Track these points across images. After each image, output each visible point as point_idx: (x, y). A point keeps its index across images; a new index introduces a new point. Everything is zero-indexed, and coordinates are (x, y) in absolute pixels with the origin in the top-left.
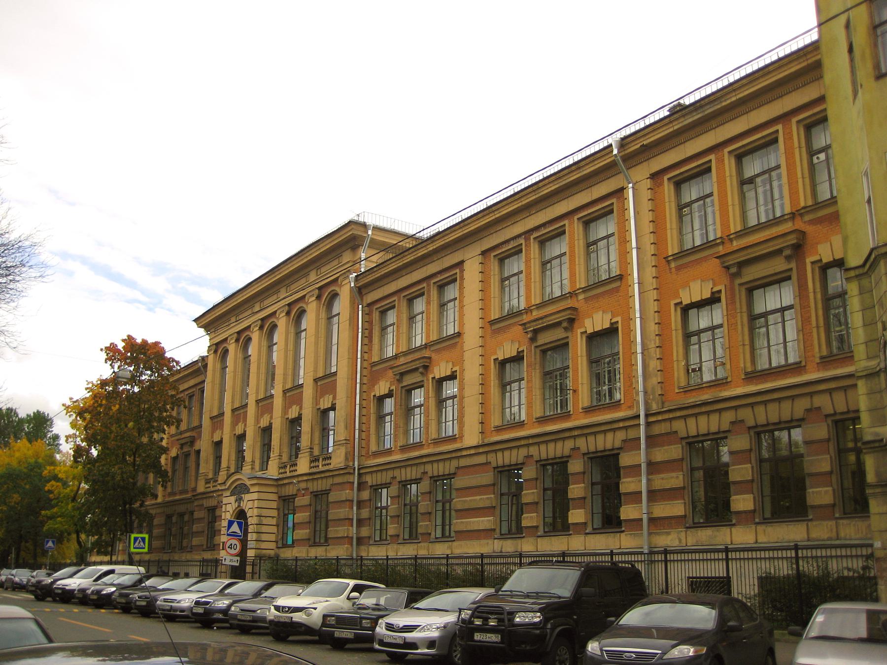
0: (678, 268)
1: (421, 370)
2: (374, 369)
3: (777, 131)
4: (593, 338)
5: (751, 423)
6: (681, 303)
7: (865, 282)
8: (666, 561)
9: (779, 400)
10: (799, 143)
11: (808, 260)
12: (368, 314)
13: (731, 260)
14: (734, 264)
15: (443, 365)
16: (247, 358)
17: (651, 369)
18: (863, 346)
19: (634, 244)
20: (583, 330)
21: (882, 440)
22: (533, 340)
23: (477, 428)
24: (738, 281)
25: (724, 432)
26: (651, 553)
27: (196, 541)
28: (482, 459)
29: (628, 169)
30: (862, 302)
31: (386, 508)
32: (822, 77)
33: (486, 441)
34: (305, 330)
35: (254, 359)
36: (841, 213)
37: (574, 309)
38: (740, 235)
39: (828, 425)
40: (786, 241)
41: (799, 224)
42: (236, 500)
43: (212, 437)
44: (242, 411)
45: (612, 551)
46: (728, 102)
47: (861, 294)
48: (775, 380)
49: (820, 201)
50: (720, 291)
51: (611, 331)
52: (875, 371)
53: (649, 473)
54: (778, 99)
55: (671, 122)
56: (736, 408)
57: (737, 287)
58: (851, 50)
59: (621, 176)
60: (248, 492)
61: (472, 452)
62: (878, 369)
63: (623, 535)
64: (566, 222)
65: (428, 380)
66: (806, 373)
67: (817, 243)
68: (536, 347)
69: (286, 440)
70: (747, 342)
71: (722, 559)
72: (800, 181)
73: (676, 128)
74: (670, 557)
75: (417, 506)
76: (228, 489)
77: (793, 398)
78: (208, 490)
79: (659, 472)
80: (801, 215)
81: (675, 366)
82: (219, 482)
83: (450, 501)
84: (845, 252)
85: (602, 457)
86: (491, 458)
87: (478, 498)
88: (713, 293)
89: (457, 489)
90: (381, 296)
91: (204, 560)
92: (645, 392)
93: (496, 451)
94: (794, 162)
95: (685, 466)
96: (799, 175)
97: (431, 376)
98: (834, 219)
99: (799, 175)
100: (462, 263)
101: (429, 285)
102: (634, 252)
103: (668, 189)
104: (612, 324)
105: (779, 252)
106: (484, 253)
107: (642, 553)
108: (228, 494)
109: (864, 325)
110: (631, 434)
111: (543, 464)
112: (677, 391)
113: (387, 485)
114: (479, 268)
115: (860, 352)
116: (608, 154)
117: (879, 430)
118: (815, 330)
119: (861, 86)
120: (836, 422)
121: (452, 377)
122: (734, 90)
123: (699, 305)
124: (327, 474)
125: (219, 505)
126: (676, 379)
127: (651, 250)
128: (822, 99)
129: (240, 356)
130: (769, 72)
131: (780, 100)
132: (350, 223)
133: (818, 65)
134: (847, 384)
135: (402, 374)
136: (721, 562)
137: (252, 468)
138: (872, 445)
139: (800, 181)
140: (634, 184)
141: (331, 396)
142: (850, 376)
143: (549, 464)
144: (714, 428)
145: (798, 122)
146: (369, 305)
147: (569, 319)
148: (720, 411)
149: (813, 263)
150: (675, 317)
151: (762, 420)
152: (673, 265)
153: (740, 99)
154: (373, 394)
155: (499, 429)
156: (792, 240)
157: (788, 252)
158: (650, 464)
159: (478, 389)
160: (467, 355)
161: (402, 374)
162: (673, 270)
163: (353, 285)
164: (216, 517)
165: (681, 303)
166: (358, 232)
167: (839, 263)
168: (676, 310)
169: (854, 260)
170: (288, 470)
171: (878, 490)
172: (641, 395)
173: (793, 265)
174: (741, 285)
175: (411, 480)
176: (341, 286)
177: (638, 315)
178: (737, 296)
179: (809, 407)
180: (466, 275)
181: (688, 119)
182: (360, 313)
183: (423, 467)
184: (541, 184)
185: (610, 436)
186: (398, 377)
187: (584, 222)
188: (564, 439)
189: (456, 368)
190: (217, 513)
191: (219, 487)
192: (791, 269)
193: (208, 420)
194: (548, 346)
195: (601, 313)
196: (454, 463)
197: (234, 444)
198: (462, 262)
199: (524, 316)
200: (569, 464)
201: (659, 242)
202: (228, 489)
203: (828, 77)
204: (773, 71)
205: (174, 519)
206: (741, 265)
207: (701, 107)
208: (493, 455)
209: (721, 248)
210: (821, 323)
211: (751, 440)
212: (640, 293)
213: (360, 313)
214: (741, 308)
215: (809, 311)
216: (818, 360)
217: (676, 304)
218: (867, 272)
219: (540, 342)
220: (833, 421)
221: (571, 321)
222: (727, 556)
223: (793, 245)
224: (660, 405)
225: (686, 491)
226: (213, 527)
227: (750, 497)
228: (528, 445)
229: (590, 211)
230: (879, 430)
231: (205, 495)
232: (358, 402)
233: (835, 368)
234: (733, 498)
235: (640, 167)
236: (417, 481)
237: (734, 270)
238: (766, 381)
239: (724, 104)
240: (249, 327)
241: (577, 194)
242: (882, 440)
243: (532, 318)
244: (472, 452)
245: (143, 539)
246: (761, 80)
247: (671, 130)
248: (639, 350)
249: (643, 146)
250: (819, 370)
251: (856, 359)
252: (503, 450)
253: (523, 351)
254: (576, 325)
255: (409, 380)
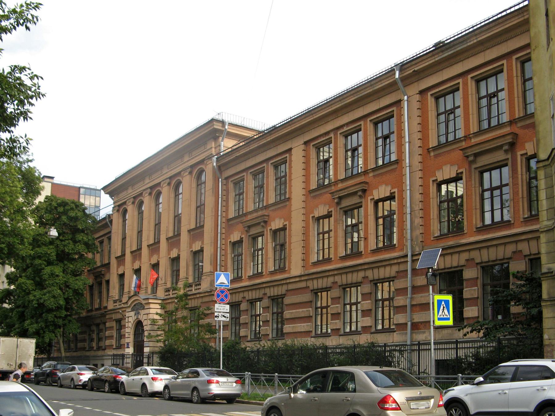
0: (436, 156)
1: (262, 224)
2: (230, 223)
3: (503, 64)
4: (275, 232)
5: (478, 261)
6: (437, 180)
7: (548, 170)
8: (419, 350)
9: (496, 245)
10: (517, 73)
11: (519, 153)
12: (225, 185)
13: (470, 152)
14: (471, 154)
15: (277, 221)
16: (141, 213)
17: (416, 224)
18: (546, 211)
19: (407, 140)
20: (372, 197)
21: (552, 272)
22: (338, 204)
23: (301, 263)
24: (474, 166)
25: (507, 259)
26: (412, 345)
27: (108, 342)
28: (303, 285)
29: (405, 87)
30: (546, 183)
31: (259, 315)
32: (528, 30)
33: (307, 272)
34: (182, 193)
35: (145, 215)
36: (537, 123)
37: (366, 183)
38: (476, 134)
39: (526, 262)
40: (505, 140)
41: (515, 129)
42: (135, 314)
43: (133, 266)
44: (138, 253)
45: (419, 342)
46: (472, 43)
47: (545, 178)
48: (494, 232)
49: (483, 129)
50: (462, 173)
51: (284, 229)
52: (551, 228)
53: (413, 293)
54: (497, 45)
55: (434, 55)
56: (469, 250)
57: (473, 170)
58: (547, 15)
59: (399, 91)
60: (144, 309)
61: (297, 279)
62: (553, 227)
63: (395, 333)
64: (362, 123)
65: (267, 231)
66: (514, 228)
67: (526, 142)
68: (341, 209)
69: (169, 272)
70: (478, 207)
71: (454, 348)
72: (516, 99)
73: (436, 59)
74: (422, 347)
75: (239, 319)
76: (129, 307)
77: (505, 244)
78: (116, 307)
79: (418, 293)
80: (516, 123)
81: (474, 212)
82: (124, 302)
83: (282, 313)
84: (538, 151)
85: (448, 273)
86: (310, 284)
87: (301, 310)
88: (457, 174)
89: (286, 305)
90: (377, 107)
91: (114, 355)
92: (412, 240)
93: (312, 279)
94: (513, 86)
95: (479, 282)
96: (516, 95)
97: (269, 228)
98: (533, 126)
99: (516, 95)
100: (290, 150)
101: (268, 165)
102: (407, 145)
103: (431, 101)
104: (391, 193)
105: (500, 147)
106: (306, 143)
107: (406, 345)
108: (130, 310)
109: (546, 199)
110: (402, 268)
111: (486, 268)
112: (432, 239)
113: (260, 300)
114: (303, 153)
115: (543, 215)
116: (390, 76)
117: (551, 266)
118: (521, 200)
119: (552, 39)
120: (531, 260)
121: (391, 198)
122: (476, 35)
123: (384, 200)
124: (198, 296)
125: (123, 318)
126: (432, 231)
127: (419, 143)
128: (528, 46)
129: (136, 213)
130: (499, 24)
131: (505, 43)
132: (212, 120)
133: (526, 22)
134: (535, 236)
135: (249, 227)
136: (453, 350)
137: (146, 292)
138: (547, 275)
139: (516, 99)
140: (408, 98)
141: (200, 242)
142: (537, 231)
143: (496, 265)
144: (500, 256)
145: (517, 59)
146: (227, 178)
147: (362, 190)
148: (459, 252)
149: (522, 155)
150: (433, 189)
151: (344, 282)
152: (432, 154)
153: (479, 41)
154: (229, 240)
155: (318, 263)
156: (509, 139)
157: (506, 147)
158: (413, 287)
159: (301, 237)
160: (293, 214)
161: (249, 227)
162: (432, 157)
163: (215, 164)
164: (121, 326)
165: (527, 154)
166: (218, 126)
167: (534, 156)
168: (433, 184)
169: (543, 155)
170: (171, 293)
171: (549, 303)
172: (409, 242)
173: (509, 156)
174: (475, 168)
175: (255, 299)
176: (206, 165)
177: (408, 188)
178: (473, 177)
179: (515, 250)
180: (293, 158)
181: (445, 53)
182: (220, 183)
183: (263, 290)
184: (345, 96)
185: (388, 269)
186: (246, 229)
187: (274, 166)
188: (328, 276)
189: (287, 223)
190: (123, 323)
191: (123, 306)
192: (508, 159)
193: (187, 233)
194: (349, 208)
195: (449, 165)
196: (285, 288)
197: (191, 258)
198: (290, 150)
199: (333, 188)
200: (464, 272)
201: (424, 138)
202: (129, 307)
203: (533, 31)
204: (486, 30)
205: (244, 306)
206: (476, 155)
207: (454, 45)
208: (311, 282)
209: (464, 143)
210: (525, 195)
211: (478, 272)
212: (410, 173)
213: (220, 183)
214: (475, 184)
215: (518, 188)
216: (522, 220)
217: (433, 181)
218: (550, 164)
219: (343, 206)
220: (529, 259)
221: (364, 191)
222: (419, 348)
223: (509, 143)
224: (421, 248)
225: (479, 300)
226: (120, 333)
227: (475, 308)
228: (334, 275)
229: (236, 177)
230: (551, 266)
231: (114, 311)
232: (219, 246)
233: (532, 225)
234: (465, 309)
235: (412, 85)
236: (327, 289)
237: (471, 158)
238: (489, 233)
239: (469, 44)
240: (160, 183)
241: (365, 107)
242: (552, 272)
243: (338, 189)
244: (297, 279)
245: (447, 302)
246: (421, 63)
247: (433, 61)
248: (408, 210)
249: (414, 71)
250: (522, 227)
251: (541, 220)
252: (317, 278)
253: (332, 211)
254: (368, 192)
255: (253, 231)
